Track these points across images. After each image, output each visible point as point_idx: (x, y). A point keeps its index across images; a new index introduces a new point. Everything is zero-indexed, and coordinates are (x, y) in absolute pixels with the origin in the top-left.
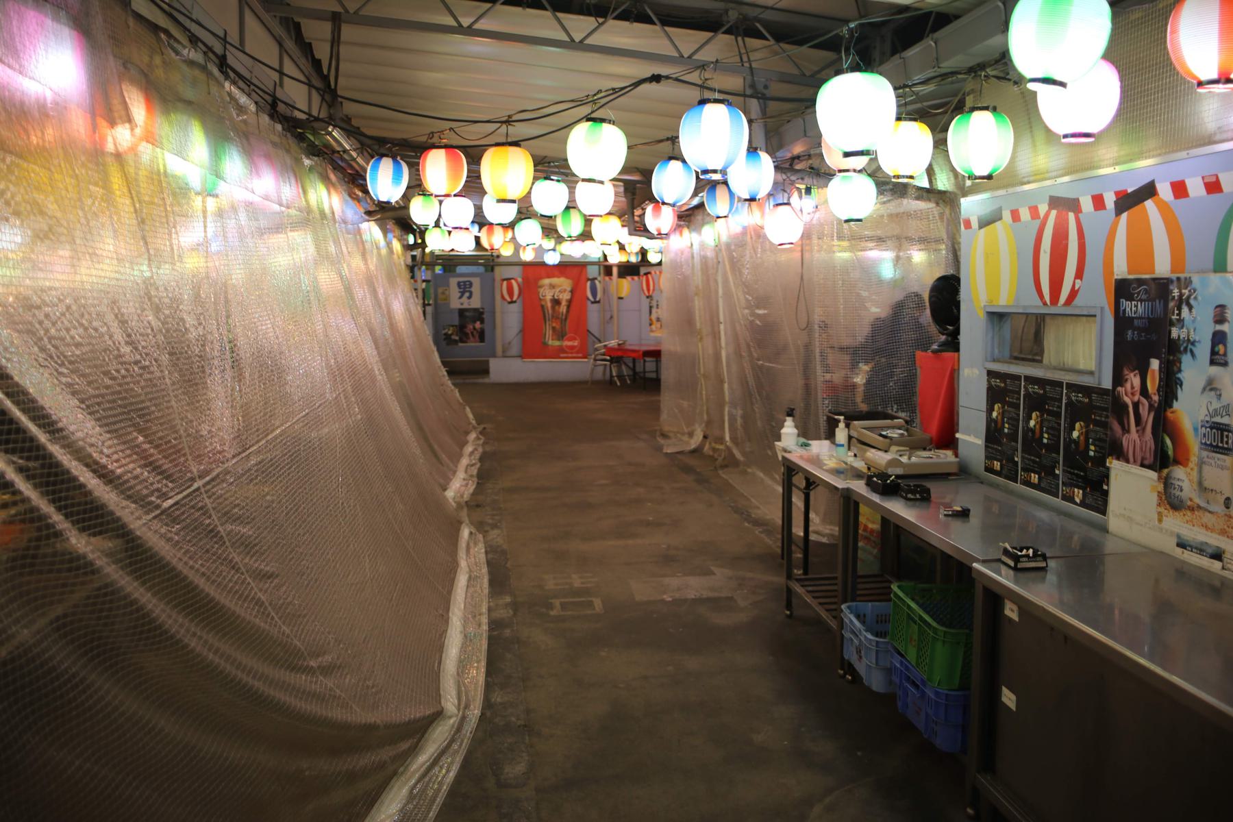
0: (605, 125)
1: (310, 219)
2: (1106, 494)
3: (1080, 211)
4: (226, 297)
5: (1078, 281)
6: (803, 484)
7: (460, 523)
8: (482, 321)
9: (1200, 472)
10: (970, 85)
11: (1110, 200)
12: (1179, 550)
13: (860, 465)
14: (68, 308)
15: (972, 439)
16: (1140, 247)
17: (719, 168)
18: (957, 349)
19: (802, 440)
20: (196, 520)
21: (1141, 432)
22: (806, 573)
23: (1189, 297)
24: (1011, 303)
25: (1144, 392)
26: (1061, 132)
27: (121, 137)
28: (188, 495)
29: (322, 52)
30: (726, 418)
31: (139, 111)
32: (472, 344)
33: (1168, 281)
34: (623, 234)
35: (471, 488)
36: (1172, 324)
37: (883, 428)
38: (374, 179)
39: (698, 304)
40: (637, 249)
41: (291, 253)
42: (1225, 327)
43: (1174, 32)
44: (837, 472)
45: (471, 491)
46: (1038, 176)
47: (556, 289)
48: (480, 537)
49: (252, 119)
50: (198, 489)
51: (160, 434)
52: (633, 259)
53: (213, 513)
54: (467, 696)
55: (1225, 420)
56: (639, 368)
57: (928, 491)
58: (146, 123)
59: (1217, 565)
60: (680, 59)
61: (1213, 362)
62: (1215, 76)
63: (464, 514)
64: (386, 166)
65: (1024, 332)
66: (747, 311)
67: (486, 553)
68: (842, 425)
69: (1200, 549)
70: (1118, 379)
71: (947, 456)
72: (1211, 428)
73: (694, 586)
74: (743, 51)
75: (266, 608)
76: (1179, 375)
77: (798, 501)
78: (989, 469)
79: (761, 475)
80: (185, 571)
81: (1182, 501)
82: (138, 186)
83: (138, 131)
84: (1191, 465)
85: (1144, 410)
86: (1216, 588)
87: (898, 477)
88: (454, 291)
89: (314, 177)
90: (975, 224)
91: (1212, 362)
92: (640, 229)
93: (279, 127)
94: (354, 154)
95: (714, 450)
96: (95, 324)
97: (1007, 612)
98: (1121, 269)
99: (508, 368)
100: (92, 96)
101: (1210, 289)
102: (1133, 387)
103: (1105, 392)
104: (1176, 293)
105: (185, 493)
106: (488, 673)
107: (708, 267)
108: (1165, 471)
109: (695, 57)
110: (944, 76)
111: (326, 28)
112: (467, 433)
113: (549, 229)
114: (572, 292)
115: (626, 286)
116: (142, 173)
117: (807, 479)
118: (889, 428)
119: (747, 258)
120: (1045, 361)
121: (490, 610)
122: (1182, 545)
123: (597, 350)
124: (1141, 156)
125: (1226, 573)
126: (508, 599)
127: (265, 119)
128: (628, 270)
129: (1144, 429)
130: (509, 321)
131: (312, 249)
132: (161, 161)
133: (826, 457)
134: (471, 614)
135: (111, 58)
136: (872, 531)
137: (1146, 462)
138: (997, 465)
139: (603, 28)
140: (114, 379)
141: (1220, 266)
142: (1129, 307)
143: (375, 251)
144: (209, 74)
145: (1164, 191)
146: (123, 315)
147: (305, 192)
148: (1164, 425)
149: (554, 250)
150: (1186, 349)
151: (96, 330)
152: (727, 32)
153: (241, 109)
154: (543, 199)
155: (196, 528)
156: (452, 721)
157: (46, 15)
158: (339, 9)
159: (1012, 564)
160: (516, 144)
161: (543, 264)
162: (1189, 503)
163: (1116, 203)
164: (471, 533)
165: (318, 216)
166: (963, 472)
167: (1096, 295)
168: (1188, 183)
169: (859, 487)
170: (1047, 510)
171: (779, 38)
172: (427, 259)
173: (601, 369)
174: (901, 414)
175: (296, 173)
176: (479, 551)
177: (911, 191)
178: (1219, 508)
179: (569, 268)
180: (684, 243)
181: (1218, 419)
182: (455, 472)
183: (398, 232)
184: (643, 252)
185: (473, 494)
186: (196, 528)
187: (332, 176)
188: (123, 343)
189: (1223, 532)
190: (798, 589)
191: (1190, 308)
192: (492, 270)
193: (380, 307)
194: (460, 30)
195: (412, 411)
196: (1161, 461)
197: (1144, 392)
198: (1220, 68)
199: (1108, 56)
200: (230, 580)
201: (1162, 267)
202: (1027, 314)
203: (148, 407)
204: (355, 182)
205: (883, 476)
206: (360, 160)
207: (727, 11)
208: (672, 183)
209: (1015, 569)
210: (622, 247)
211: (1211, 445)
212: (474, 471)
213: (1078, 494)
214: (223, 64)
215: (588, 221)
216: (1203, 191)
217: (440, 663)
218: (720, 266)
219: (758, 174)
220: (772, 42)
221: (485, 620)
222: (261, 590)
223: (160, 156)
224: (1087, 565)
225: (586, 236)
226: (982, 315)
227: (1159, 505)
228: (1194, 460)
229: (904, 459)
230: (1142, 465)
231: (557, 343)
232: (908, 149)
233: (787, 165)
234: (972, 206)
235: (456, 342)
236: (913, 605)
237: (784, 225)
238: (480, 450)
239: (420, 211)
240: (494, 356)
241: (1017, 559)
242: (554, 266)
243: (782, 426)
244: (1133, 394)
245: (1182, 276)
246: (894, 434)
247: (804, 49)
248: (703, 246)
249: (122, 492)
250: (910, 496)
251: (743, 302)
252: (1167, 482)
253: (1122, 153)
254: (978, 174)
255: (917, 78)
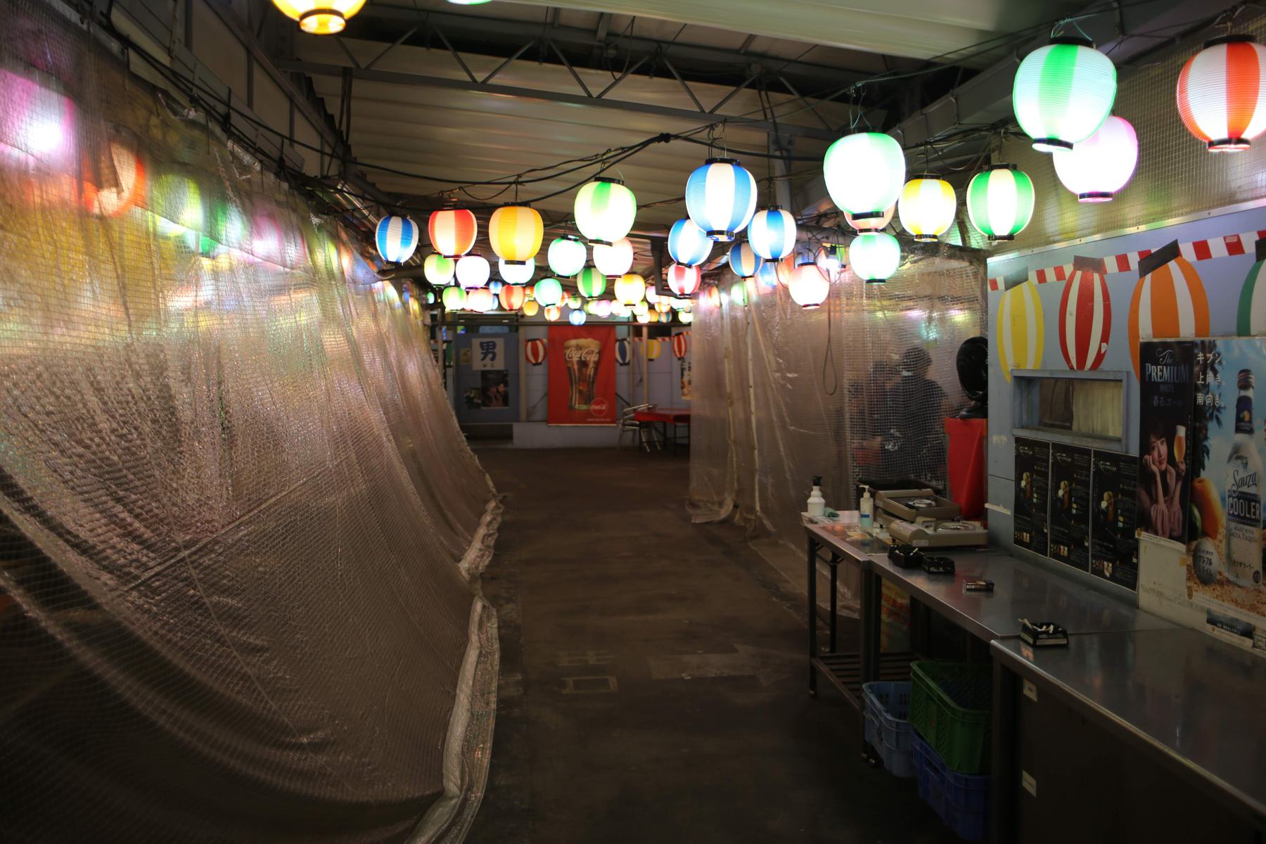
0: (613, 186)
1: (315, 279)
2: (1135, 567)
3: (1105, 272)
4: (219, 362)
5: (1104, 345)
6: (829, 557)
7: (473, 596)
8: (506, 384)
9: (1228, 544)
10: (995, 142)
11: (1134, 260)
12: (1209, 627)
13: (885, 536)
14: (39, 376)
15: (1000, 509)
16: (1165, 309)
17: (725, 228)
18: (985, 416)
19: (830, 510)
20: (178, 591)
21: (1169, 502)
22: (833, 650)
23: (1213, 361)
24: (1038, 367)
25: (1171, 459)
26: (1078, 191)
27: (108, 200)
28: (171, 566)
29: (334, 107)
30: (757, 487)
31: (128, 175)
32: (496, 407)
33: (1193, 344)
34: (652, 295)
35: (487, 561)
36: (1197, 389)
37: (910, 498)
38: (383, 239)
39: (728, 367)
40: (666, 309)
41: (299, 314)
42: (1250, 393)
43: (1183, 91)
44: (862, 545)
45: (487, 562)
46: (1068, 235)
47: (584, 350)
48: (494, 612)
49: (257, 178)
50: (183, 559)
51: (140, 503)
52: (664, 319)
53: (199, 584)
54: (470, 776)
55: (1252, 490)
56: (670, 434)
57: (952, 564)
58: (136, 187)
59: (1247, 643)
60: (701, 115)
61: (1238, 430)
62: (1225, 136)
63: (478, 585)
64: (395, 225)
65: (1050, 396)
66: (778, 375)
67: (499, 628)
68: (867, 495)
69: (1231, 625)
70: (1146, 447)
71: (976, 527)
72: (1239, 498)
73: (715, 664)
74: (766, 105)
75: (252, 682)
76: (1206, 443)
77: (823, 571)
78: (1019, 541)
79: (793, 547)
80: (158, 647)
81: (1211, 575)
82: (122, 251)
83: (126, 194)
84: (1219, 537)
85: (1171, 479)
86: (1247, 666)
87: (921, 549)
88: (477, 352)
89: (324, 237)
90: (1001, 285)
91: (1238, 430)
92: (664, 290)
93: (285, 186)
94: (365, 212)
95: (747, 520)
96: (67, 391)
97: (1026, 692)
98: (1146, 332)
99: (531, 434)
100: (80, 161)
101: (1234, 351)
102: (1160, 456)
103: (1133, 460)
104: (1201, 357)
105: (167, 564)
106: (494, 755)
107: (738, 327)
108: (1194, 543)
109: (717, 112)
110: (966, 133)
111: (336, 84)
112: (486, 502)
113: (569, 286)
114: (599, 353)
115: (656, 347)
116: (128, 237)
117: (834, 555)
118: (916, 497)
119: (777, 318)
120: (1075, 427)
121: (499, 687)
122: (1212, 621)
123: (625, 414)
124: (1166, 214)
125: (1256, 651)
126: (519, 677)
127: (271, 178)
128: (657, 330)
129: (1172, 499)
130: (534, 383)
131: (317, 312)
132: (151, 224)
133: (853, 526)
134: (479, 692)
135: (102, 122)
136: (902, 606)
137: (1175, 534)
138: (1026, 537)
139: (621, 83)
140: (87, 447)
141: (1243, 329)
142: (1155, 372)
143: (388, 312)
144: (210, 134)
145: (1187, 252)
146: (98, 383)
147: (311, 252)
148: (1192, 495)
149: (579, 310)
150: (1211, 415)
151: (69, 398)
152: (751, 86)
153: (245, 169)
154: (568, 260)
155: (178, 599)
156: (453, 802)
157: (34, 81)
158: (350, 65)
159: (1031, 641)
160: (525, 204)
161: (569, 325)
162: (1218, 577)
163: (1140, 263)
164: (484, 607)
165: (325, 276)
166: (992, 544)
167: (1121, 359)
168: (1211, 243)
169: (882, 560)
170: (1080, 583)
171: (804, 92)
172: (449, 319)
173: (630, 434)
174: (934, 483)
175: (301, 230)
176: (493, 627)
177: (944, 250)
178: (1248, 582)
179: (594, 327)
180: (712, 301)
181: (1245, 489)
182: (470, 543)
183: (416, 291)
184: (674, 313)
185: (487, 566)
186: (178, 599)
187: (344, 236)
188: (99, 412)
189: (1253, 608)
190: (822, 668)
191: (1215, 372)
192: (517, 330)
193: (391, 371)
194: (474, 85)
195: (421, 476)
196: (1190, 533)
197: (1171, 459)
198: (1229, 128)
199: (1118, 110)
200: (213, 654)
201: (1187, 329)
202: (1057, 379)
203: (125, 476)
204: (364, 241)
205: (907, 548)
206: (371, 218)
207: (749, 65)
208: (688, 243)
209: (1034, 646)
210: (651, 307)
211: (1239, 516)
212: (491, 542)
213: (1108, 568)
214: (225, 122)
215: (611, 280)
216: (1225, 253)
217: (444, 740)
218: (750, 327)
219: (776, 234)
220: (797, 96)
221: (493, 698)
222: (248, 664)
223: (150, 218)
224: (1117, 640)
225: (609, 295)
226: (1009, 379)
227: (1189, 579)
228: (1222, 531)
229: (930, 531)
230: (1171, 537)
231: (584, 407)
232: (930, 207)
233: (813, 223)
234: (997, 264)
235: (478, 406)
236: (932, 684)
237: (809, 287)
238: (499, 519)
239: (434, 272)
240: (518, 421)
241: (1036, 635)
242: (579, 326)
243: (810, 496)
244: (1161, 463)
245: (1206, 339)
246: (922, 504)
247: (826, 103)
248: (732, 306)
249: (97, 562)
250: (932, 569)
251: (774, 364)
252: (1196, 555)
253: (1145, 212)
254: (997, 234)
255: (939, 135)
